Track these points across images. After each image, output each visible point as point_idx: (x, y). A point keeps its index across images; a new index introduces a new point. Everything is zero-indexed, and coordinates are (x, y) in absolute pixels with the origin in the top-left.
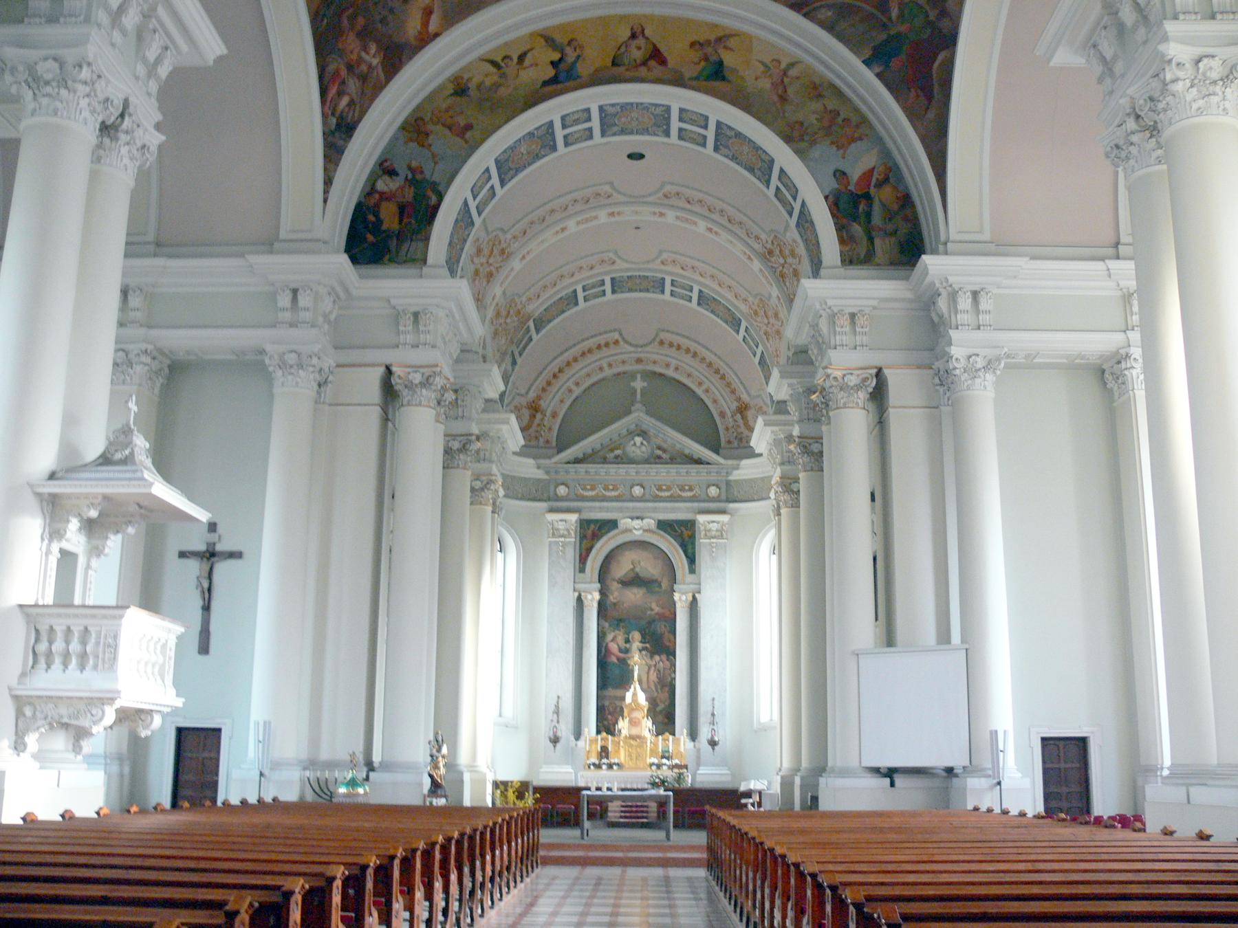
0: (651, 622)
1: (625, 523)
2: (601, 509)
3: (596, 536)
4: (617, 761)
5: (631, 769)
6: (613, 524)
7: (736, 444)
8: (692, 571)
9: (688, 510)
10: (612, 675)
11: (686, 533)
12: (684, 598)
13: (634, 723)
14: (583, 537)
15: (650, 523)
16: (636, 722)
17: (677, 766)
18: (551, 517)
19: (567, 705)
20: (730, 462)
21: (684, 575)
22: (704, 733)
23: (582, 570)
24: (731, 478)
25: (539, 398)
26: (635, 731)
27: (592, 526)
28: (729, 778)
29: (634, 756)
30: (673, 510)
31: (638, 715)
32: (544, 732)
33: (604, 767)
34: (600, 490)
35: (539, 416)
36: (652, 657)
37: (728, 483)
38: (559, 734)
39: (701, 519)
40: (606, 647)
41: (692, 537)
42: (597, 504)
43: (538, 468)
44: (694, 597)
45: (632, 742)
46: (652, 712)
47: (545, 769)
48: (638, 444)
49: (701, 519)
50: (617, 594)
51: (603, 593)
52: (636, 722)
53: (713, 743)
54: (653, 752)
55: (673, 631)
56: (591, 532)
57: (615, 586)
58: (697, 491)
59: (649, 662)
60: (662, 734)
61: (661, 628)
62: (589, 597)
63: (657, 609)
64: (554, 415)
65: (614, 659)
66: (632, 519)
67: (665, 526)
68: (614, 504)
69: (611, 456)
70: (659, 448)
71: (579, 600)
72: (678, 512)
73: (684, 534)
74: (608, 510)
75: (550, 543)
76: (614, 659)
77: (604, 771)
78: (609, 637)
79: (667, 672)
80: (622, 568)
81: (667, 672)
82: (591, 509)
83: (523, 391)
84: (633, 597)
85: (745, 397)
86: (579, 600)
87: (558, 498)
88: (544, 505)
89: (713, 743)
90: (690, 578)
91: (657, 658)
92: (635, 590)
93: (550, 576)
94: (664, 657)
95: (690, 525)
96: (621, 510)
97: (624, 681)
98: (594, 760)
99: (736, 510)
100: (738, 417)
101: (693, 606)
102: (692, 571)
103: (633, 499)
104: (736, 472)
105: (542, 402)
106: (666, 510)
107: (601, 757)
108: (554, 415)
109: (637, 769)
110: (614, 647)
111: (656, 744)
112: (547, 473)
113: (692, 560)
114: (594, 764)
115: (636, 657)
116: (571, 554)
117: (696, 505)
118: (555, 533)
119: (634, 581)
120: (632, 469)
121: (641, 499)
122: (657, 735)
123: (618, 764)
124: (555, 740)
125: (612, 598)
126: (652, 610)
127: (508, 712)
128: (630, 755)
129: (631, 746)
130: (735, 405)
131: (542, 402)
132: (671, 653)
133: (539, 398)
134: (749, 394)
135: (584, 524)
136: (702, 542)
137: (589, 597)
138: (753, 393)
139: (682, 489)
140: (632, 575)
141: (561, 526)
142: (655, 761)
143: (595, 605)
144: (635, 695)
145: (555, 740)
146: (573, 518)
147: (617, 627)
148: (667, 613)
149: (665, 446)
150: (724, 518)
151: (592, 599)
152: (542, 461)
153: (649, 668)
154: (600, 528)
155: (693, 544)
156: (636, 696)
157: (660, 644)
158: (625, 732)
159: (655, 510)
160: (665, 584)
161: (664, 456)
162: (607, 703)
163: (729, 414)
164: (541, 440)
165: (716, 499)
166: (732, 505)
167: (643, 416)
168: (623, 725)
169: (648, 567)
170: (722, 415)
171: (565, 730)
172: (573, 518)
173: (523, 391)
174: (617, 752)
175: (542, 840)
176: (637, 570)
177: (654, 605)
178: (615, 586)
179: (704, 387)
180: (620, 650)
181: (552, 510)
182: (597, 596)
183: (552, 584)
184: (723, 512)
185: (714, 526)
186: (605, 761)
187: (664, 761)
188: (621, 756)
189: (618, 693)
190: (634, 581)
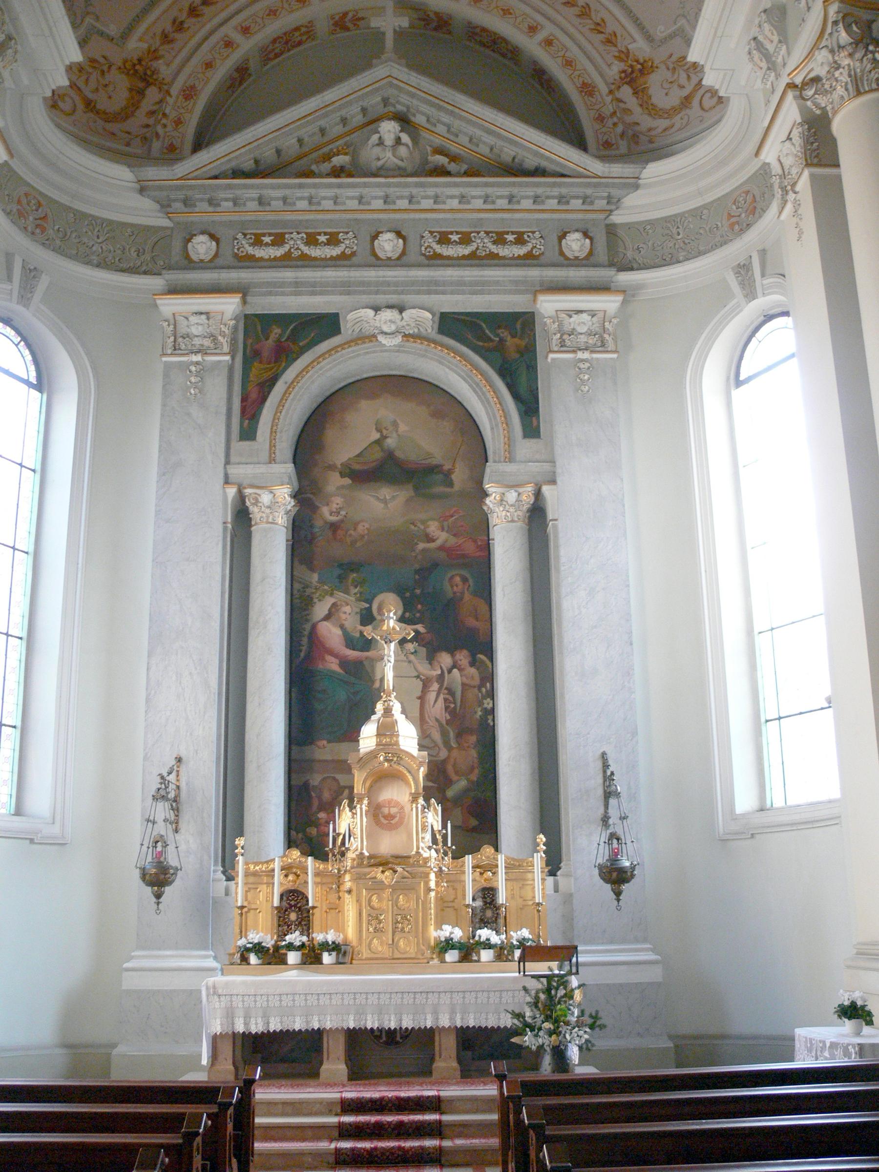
0: (428, 570)
1: (358, 318)
2: (298, 288)
3: (284, 354)
4: (331, 937)
5: (378, 962)
6: (327, 325)
7: (623, 149)
8: (532, 431)
9: (519, 286)
10: (324, 702)
11: (510, 342)
12: (511, 496)
13: (382, 818)
14: (251, 356)
15: (420, 318)
16: (393, 816)
17: (532, 952)
18: (170, 305)
19: (203, 776)
20: (617, 169)
21: (510, 442)
22: (585, 848)
23: (248, 434)
24: (617, 218)
25: (154, 54)
26: (388, 845)
27: (276, 331)
28: (655, 974)
29: (387, 919)
30: (479, 287)
31: (397, 795)
32: (134, 853)
33: (293, 957)
34: (296, 243)
35: (152, 94)
36: (431, 658)
37: (611, 230)
38: (172, 860)
39: (548, 305)
40: (313, 633)
41: (529, 353)
42: (288, 275)
43: (142, 190)
44: (538, 494)
45: (378, 873)
46: (437, 786)
47: (141, 960)
48: (389, 140)
49: (548, 305)
50: (337, 502)
51: (306, 497)
52: (393, 816)
53: (616, 876)
54: (447, 909)
55: (484, 589)
56: (272, 345)
57: (335, 482)
58: (534, 244)
59: (424, 668)
60: (474, 849)
61: (453, 583)
62: (266, 498)
63: (442, 537)
64: (189, 93)
65: (333, 665)
66: (377, 309)
67: (455, 326)
68: (330, 274)
69: (326, 167)
70: (440, 151)
71: (242, 517)
72: (490, 293)
73: (507, 346)
74: (315, 288)
75: (168, 366)
76: (333, 665)
77: (292, 976)
78: (321, 609)
79: (472, 694)
80: (351, 440)
81: (472, 694)
82: (274, 288)
83: (113, 30)
84: (382, 507)
85: (640, 47)
86: (242, 517)
87: (189, 264)
88: (157, 282)
89: (616, 876)
90: (525, 448)
91: (445, 659)
92: (386, 492)
93: (166, 447)
94: (463, 657)
95: (523, 323)
96: (346, 288)
97: (361, 701)
98: (262, 933)
99: (640, 287)
100: (626, 92)
101: (537, 516)
102: (532, 431)
103: (377, 261)
104: (632, 200)
105: (160, 65)
106: (459, 287)
107: (283, 926)
108: (189, 93)
109: (396, 961)
110: (331, 634)
111: (453, 881)
112: (165, 206)
113: (529, 406)
114: (258, 949)
115: (390, 651)
116: (218, 395)
117: (534, 273)
118: (178, 342)
119: (383, 469)
120: (374, 190)
121: (400, 261)
122: (457, 856)
123: (335, 948)
124: (158, 878)
125: (327, 513)
126: (430, 539)
127: (41, 800)
128: (375, 917)
129: (377, 887)
130: (615, 69)
131: (160, 65)
132: (481, 647)
133: (154, 54)
134: (649, 38)
135: (255, 325)
136: (552, 360)
137: (266, 498)
138: (660, 31)
139: (500, 239)
140: (377, 455)
141: (197, 327)
142: (458, 934)
143: (282, 520)
144: (387, 730)
145: (158, 878)
146: (228, 306)
147: (341, 582)
148: (470, 548)
149: (454, 148)
150: (609, 303)
151: (275, 506)
152: (152, 172)
153: (426, 684)
154: (294, 337)
155: (532, 368)
156: (397, 731)
157: (453, 625)
158: (357, 846)
159: (433, 287)
160: (460, 476)
161: (452, 167)
162: (315, 780)
163: (603, 88)
164: (156, 145)
165: (588, 261)
166: (624, 278)
167: (401, 72)
168: (349, 822)
169: (415, 435)
170: (587, 89)
171: (192, 847)
172: (228, 306)
173: (113, 30)
174: (336, 908)
175: (206, 1074)
176: (391, 442)
177: (433, 528)
178: (335, 482)
179: (541, 36)
180: (350, 642)
181: (174, 290)
182: (284, 494)
183: (169, 467)
184: (603, 288)
185: (582, 323)
186: (295, 937)
187: (484, 933)
188: (344, 921)
189: (340, 750)
190: (383, 469)
